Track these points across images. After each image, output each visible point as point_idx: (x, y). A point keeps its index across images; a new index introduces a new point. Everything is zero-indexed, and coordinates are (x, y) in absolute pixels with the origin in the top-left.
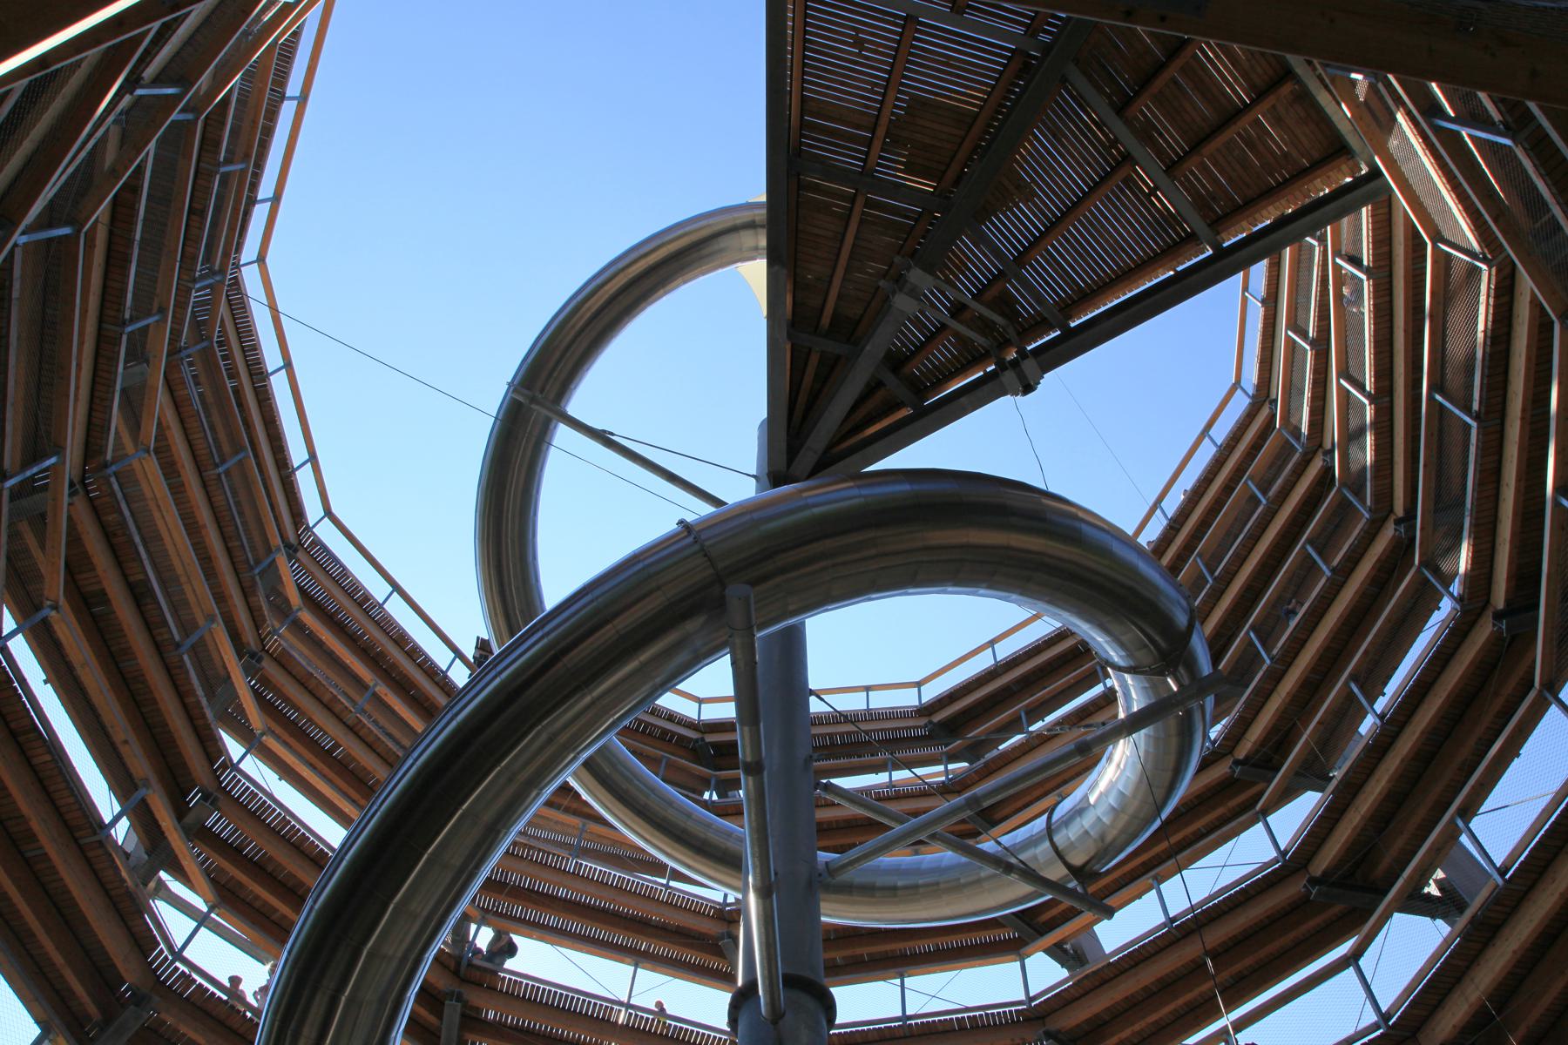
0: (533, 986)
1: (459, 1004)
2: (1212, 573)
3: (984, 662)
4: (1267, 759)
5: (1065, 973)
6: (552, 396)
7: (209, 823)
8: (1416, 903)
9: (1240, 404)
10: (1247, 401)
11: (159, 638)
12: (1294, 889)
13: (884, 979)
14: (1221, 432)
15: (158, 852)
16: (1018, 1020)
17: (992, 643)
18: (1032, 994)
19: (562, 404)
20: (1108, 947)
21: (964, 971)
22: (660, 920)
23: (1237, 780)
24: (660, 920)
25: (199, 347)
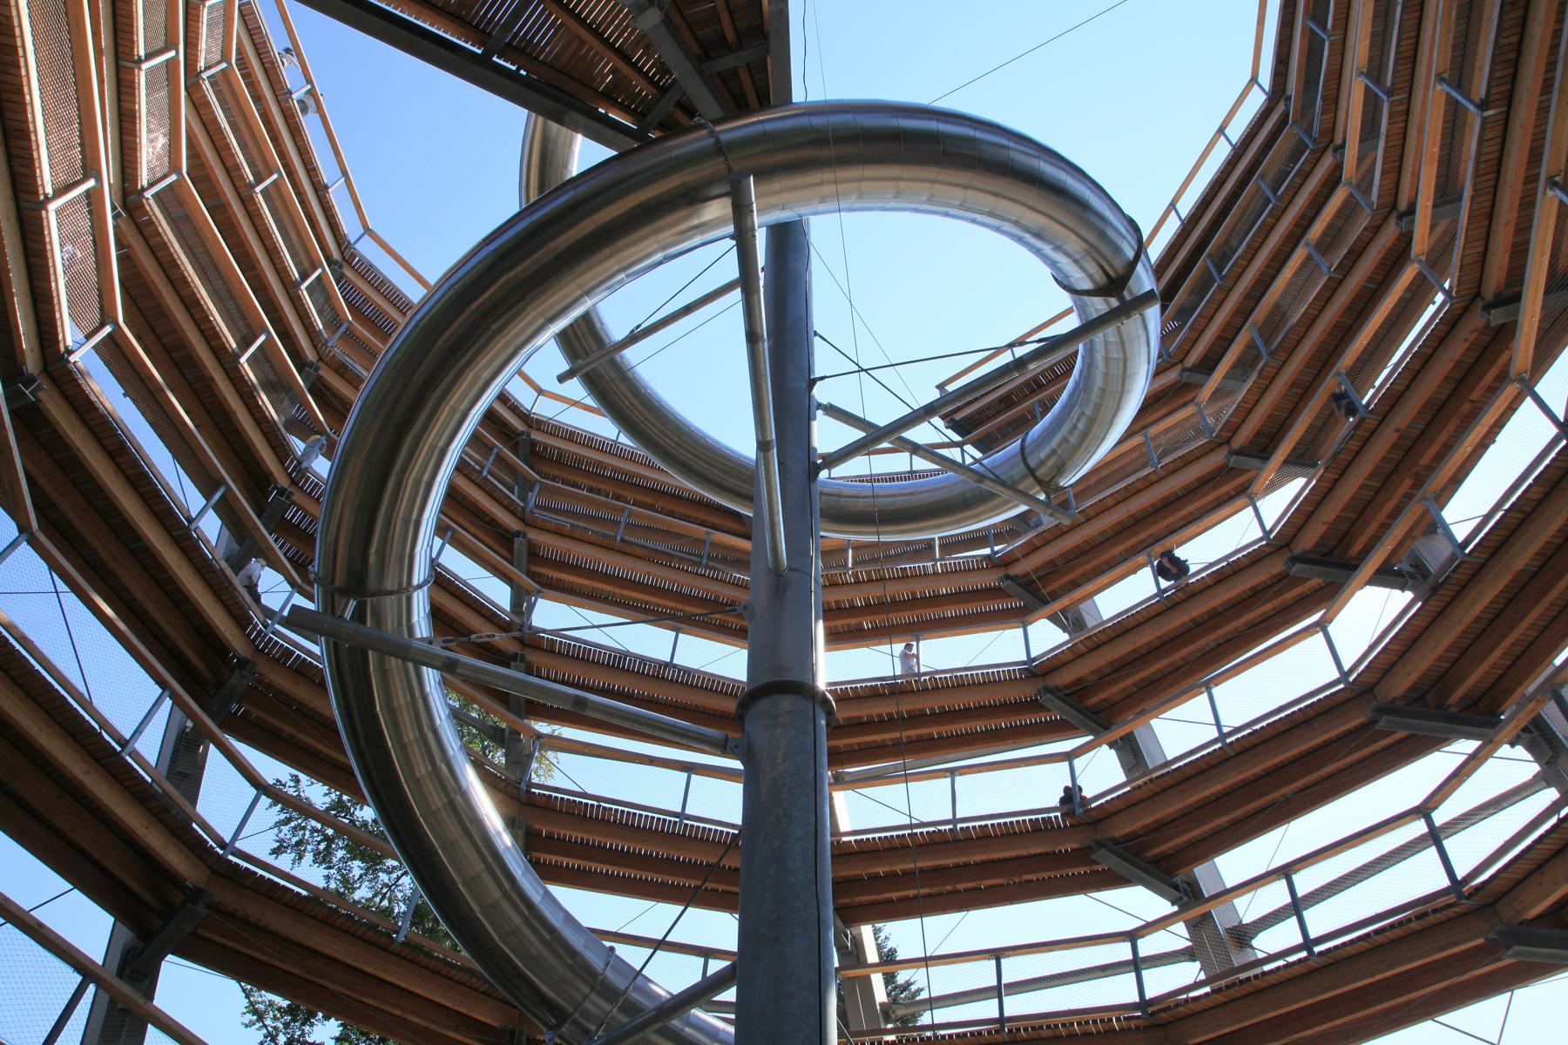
0: (575, 646)
1: (523, 664)
2: (1220, 271)
3: (1222, 152)
4: (1263, 447)
5: (1066, 637)
6: (594, 347)
7: (288, 516)
8: (1387, 576)
9: (1257, 100)
10: (1263, 97)
11: (23, 204)
12: (1276, 567)
13: (868, 646)
14: (1236, 131)
15: (246, 546)
16: (1021, 678)
17: (1221, 130)
18: (1033, 656)
19: (607, 341)
20: (1106, 615)
21: (1007, 632)
22: (643, 693)
23: (1232, 468)
24: (643, 693)
25: (492, 458)
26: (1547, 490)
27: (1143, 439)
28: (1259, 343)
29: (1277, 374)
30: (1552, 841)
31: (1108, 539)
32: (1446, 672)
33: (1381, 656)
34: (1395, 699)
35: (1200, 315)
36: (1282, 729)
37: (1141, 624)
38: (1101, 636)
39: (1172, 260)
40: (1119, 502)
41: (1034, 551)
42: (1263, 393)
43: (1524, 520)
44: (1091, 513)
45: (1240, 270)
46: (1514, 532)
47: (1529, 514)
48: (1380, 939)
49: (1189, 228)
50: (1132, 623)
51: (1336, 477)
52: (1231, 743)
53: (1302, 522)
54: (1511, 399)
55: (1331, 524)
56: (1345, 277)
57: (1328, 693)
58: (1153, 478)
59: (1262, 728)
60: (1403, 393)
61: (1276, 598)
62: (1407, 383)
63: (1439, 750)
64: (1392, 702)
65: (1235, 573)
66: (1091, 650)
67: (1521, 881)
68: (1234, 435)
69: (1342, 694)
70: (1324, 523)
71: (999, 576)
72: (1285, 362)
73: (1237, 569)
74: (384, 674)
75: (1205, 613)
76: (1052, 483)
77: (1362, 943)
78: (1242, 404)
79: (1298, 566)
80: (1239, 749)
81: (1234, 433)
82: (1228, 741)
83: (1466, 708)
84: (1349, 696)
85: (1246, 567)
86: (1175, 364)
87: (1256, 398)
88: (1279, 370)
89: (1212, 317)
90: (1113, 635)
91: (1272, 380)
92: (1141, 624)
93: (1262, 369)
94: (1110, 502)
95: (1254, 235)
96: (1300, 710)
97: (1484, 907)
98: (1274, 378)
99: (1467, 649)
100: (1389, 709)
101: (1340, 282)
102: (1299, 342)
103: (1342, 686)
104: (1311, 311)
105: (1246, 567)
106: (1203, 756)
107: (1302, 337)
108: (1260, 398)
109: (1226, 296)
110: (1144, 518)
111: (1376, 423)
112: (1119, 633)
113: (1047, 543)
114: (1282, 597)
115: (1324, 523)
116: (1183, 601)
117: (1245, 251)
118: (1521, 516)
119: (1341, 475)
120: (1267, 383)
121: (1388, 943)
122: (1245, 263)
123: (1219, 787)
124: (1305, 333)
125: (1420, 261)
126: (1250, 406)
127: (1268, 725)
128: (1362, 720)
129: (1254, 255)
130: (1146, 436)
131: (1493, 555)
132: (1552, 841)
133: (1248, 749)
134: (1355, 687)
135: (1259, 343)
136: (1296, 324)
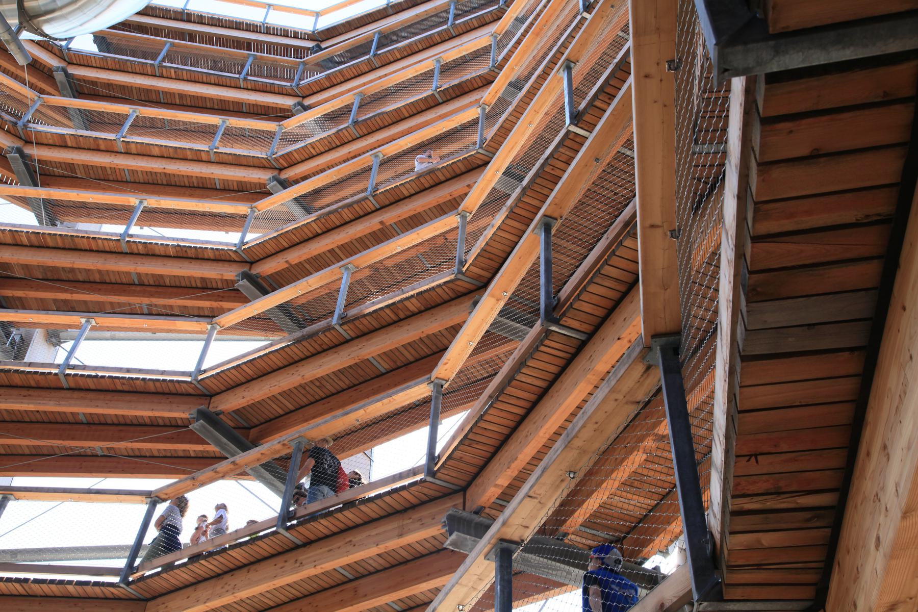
12: (230, 273)
26: (423, 308)
27: (221, 122)
28: (355, 108)
29: (350, 142)
30: (215, 563)
31: (135, 182)
32: (276, 418)
33: (232, 371)
34: (222, 412)
35: (340, 71)
36: (120, 388)
37: (91, 251)
38: (48, 239)
39: (361, 26)
40: (162, 157)
41: (61, 146)
42: (330, 150)
43: (395, 322)
44: (133, 149)
45: (392, 60)
46: (383, 327)
47: (401, 320)
48: (36, 588)
49: (391, 11)
50: (84, 244)
51: (319, 231)
52: (69, 375)
53: (273, 252)
54: (448, 228)
55: (292, 266)
56: (444, 102)
57: (175, 378)
58: (204, 157)
59: (103, 377)
60: (405, 198)
61: (216, 301)
62: (413, 192)
63: (236, 481)
64: (218, 414)
65: (197, 259)
66: (32, 246)
67: (178, 589)
68: (289, 167)
69: (184, 385)
70: (287, 262)
71: (12, 145)
72: (361, 137)
73: (200, 256)
74: (30, 365)
75: (153, 275)
76: (35, 21)
77: (17, 585)
78: (309, 147)
79: (245, 282)
80: (72, 385)
81: (290, 166)
82: (68, 372)
83: (239, 428)
84: (191, 391)
85: (208, 260)
86: (299, 96)
87: (323, 150)
88: (354, 140)
89: (349, 80)
90: (60, 245)
91: (343, 144)
92: (91, 251)
93: (341, 130)
94: (156, 151)
95: (419, 41)
96: (144, 379)
97: (140, 600)
98: (345, 143)
99: (302, 407)
100: (212, 419)
101: (438, 104)
102: (381, 128)
103: (189, 379)
104: (404, 111)
105: (208, 260)
106: (36, 373)
107: (385, 127)
108: (326, 151)
109: (370, 71)
110: (176, 186)
111: (373, 209)
112: (67, 246)
113: (78, 148)
114: (221, 303)
115: (287, 262)
116: (139, 254)
117: (404, 47)
118: (394, 318)
119: (324, 233)
120: (338, 144)
121: (41, 596)
122: (399, 57)
123: (31, 407)
124: (390, 125)
125: (484, 109)
126: (314, 153)
127: (110, 377)
128: (185, 415)
129: (409, 55)
130: (224, 122)
131: (358, 337)
132: (215, 563)
133: (80, 389)
134: (198, 386)
135: (355, 108)
136: (387, 113)
